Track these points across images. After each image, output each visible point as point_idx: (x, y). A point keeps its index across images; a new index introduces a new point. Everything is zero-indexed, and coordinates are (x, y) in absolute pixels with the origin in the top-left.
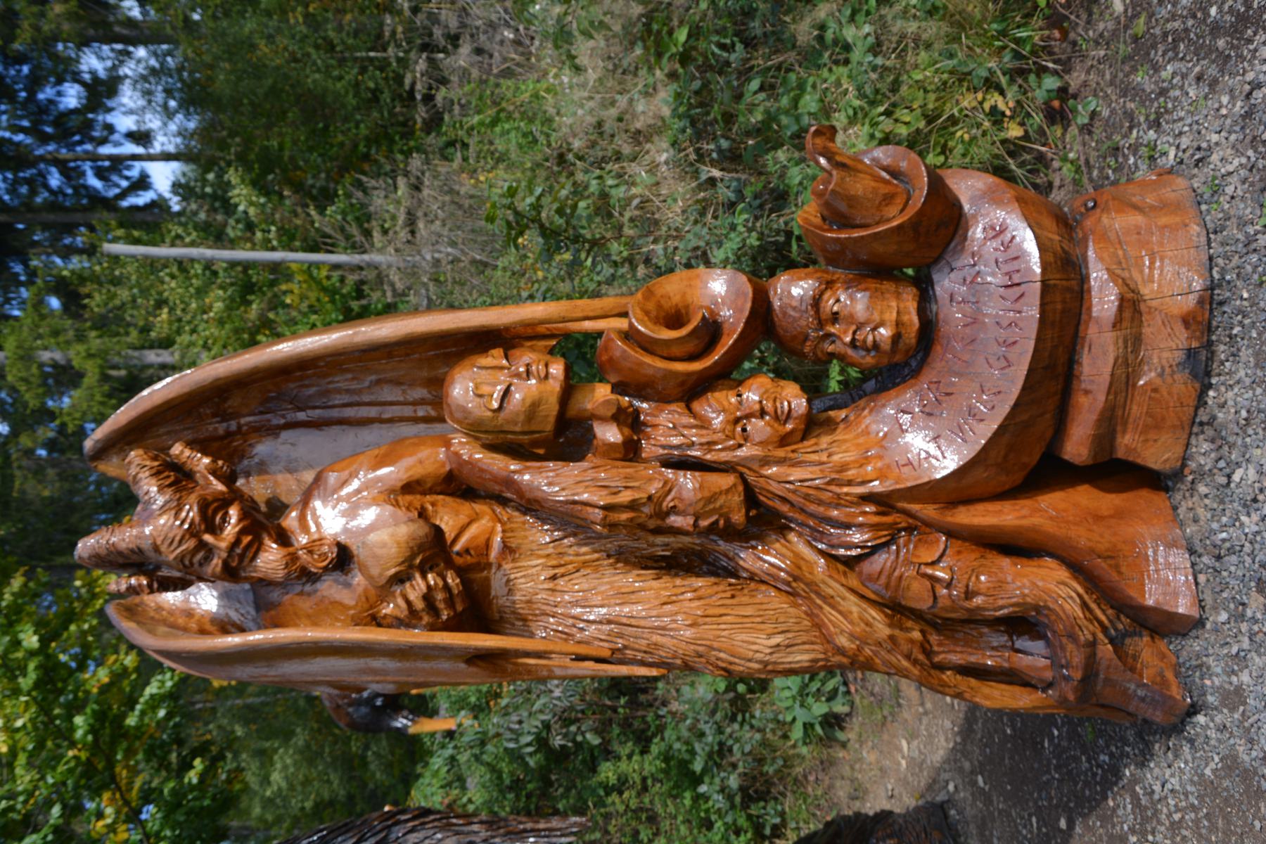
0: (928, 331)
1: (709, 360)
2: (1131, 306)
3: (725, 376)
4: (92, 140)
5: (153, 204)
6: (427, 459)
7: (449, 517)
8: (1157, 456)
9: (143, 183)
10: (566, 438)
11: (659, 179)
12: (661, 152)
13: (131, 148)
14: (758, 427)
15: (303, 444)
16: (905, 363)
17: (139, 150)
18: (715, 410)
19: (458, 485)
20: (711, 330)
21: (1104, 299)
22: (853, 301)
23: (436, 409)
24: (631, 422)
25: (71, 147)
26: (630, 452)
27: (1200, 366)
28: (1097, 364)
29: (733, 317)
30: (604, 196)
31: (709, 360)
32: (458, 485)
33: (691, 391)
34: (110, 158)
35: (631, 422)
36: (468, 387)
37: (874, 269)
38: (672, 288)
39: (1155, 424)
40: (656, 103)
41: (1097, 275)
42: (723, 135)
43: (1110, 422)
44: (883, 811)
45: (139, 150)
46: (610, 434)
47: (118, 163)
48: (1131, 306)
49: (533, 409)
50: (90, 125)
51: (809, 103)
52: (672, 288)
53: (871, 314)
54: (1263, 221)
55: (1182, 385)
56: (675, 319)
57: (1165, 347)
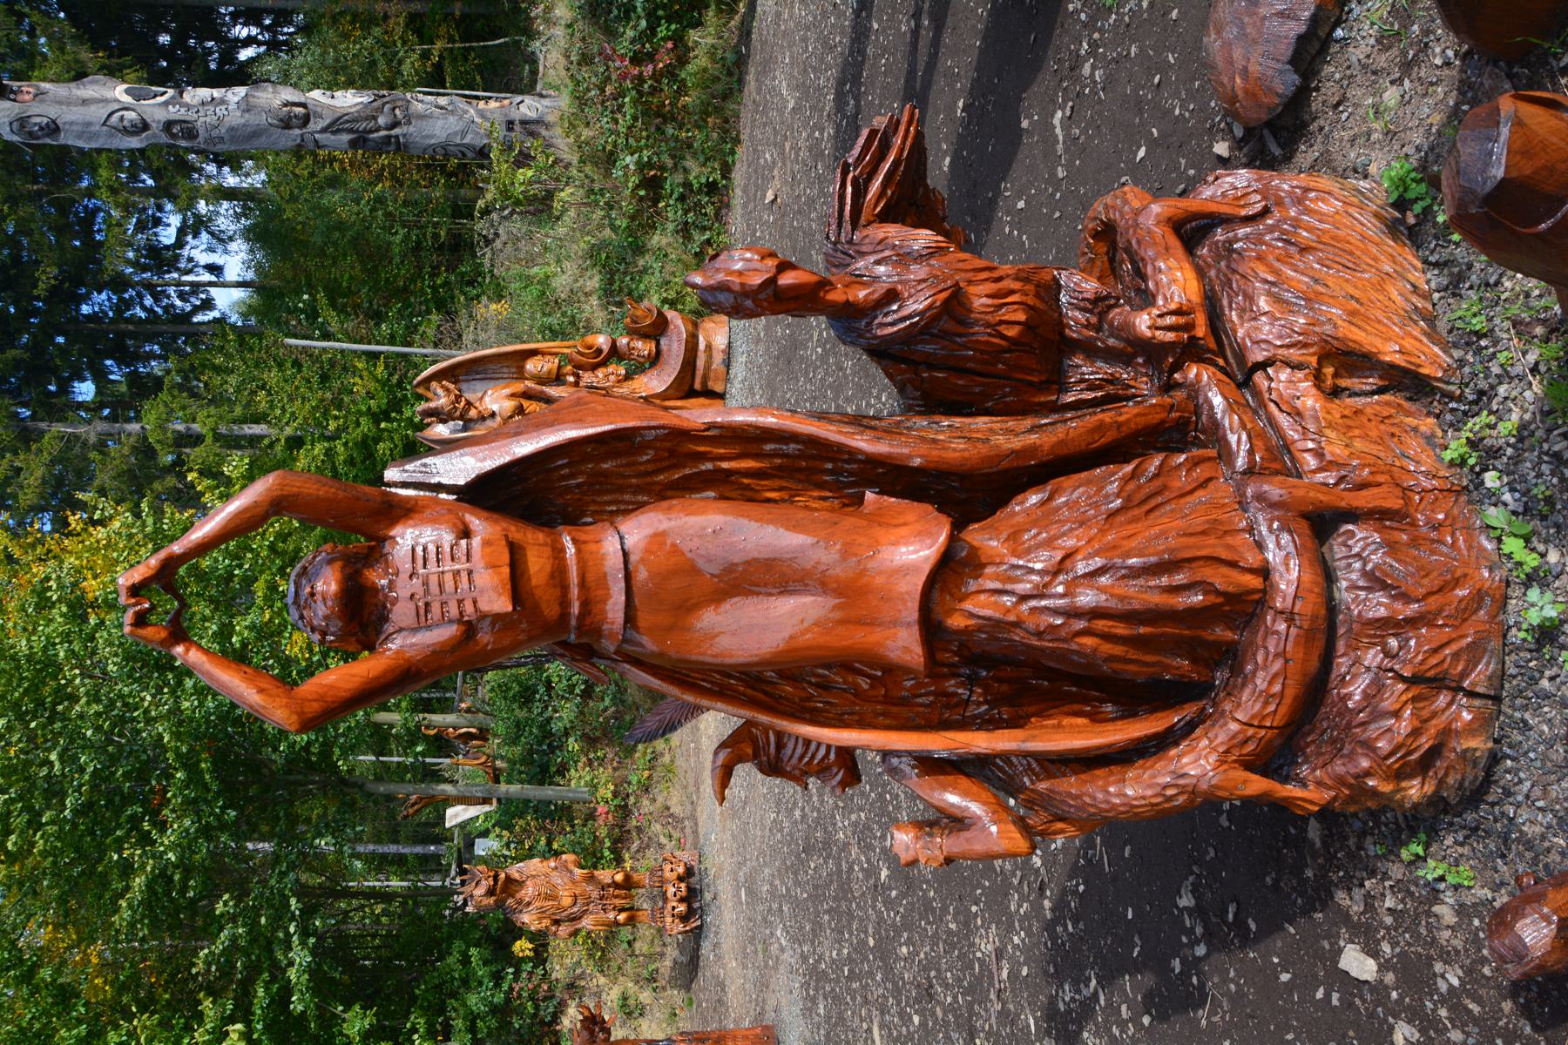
0: (658, 352)
1: (601, 359)
2: (709, 347)
3: (604, 364)
4: (178, 270)
5: (216, 320)
6: (519, 387)
7: (525, 403)
8: (718, 388)
9: (208, 304)
10: (558, 379)
11: (593, 309)
12: (594, 301)
13: (207, 277)
14: (612, 378)
15: (479, 385)
16: (655, 359)
17: (213, 278)
18: (600, 373)
19: (527, 395)
20: (599, 351)
21: (702, 346)
22: (639, 344)
23: (521, 375)
24: (577, 376)
25: (160, 273)
26: (576, 384)
27: (728, 364)
28: (701, 362)
29: (606, 348)
30: (573, 317)
31: (601, 359)
32: (527, 395)
33: (594, 368)
34: (192, 284)
35: (577, 376)
36: (531, 366)
37: (645, 336)
38: (589, 339)
39: (717, 379)
40: (594, 282)
41: (701, 338)
42: (611, 294)
43: (705, 378)
44: (762, 771)
45: (213, 278)
46: (571, 379)
47: (197, 287)
48: (709, 347)
49: (550, 372)
50: (177, 258)
51: (642, 287)
52: (589, 339)
53: (643, 347)
54: (1565, 429)
55: (723, 369)
56: (590, 348)
57: (718, 358)
